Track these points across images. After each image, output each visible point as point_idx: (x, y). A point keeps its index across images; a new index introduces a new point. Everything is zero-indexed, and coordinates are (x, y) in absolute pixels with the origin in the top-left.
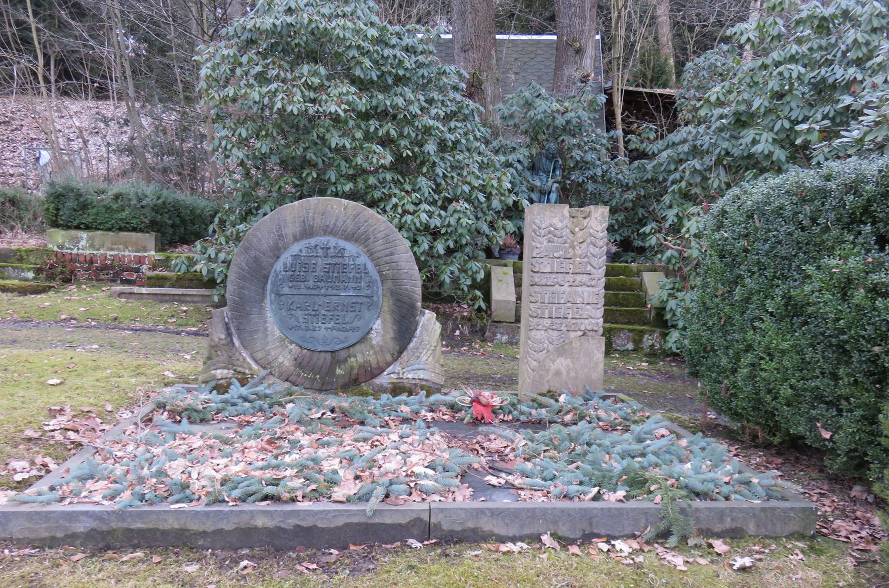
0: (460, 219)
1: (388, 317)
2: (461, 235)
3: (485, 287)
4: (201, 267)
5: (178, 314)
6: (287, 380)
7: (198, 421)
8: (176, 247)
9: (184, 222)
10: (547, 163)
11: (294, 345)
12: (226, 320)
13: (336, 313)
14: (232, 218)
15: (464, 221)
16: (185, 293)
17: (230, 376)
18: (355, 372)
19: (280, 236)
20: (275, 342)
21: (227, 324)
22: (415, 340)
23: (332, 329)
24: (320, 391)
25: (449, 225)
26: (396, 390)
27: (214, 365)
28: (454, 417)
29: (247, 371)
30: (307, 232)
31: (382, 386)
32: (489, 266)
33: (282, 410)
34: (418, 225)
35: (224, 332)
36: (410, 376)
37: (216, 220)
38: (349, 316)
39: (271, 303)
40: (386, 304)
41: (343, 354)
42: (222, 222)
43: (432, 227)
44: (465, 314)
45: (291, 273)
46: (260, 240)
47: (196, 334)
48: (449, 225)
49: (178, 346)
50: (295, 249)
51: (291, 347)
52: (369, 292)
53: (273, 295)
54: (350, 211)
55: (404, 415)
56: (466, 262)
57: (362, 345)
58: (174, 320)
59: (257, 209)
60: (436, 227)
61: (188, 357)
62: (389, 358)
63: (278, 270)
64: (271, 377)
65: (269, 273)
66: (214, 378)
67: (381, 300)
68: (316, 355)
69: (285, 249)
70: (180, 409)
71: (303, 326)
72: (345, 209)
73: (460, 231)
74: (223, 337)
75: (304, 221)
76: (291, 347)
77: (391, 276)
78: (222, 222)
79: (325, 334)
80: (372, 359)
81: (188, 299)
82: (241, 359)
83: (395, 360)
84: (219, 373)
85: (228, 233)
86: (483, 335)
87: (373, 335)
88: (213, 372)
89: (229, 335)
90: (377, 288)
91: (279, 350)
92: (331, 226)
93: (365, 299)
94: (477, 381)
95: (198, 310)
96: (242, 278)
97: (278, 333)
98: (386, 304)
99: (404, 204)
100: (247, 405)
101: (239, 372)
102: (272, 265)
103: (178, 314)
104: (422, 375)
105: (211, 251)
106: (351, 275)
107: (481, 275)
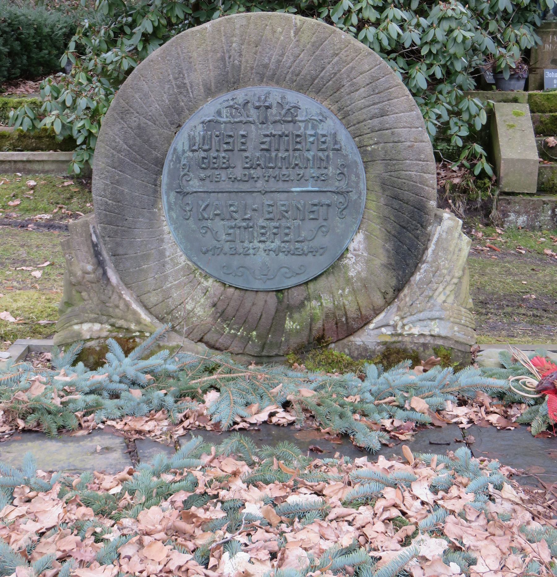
0: (451, 31)
1: (376, 227)
2: (455, 57)
3: (487, 137)
4: (52, 121)
5: (23, 192)
6: (201, 340)
7: (54, 432)
8: (17, 86)
9: (26, 47)
11: (211, 280)
12: (94, 239)
13: (284, 223)
14: (95, 41)
15: (459, 34)
16: (31, 158)
17: (105, 334)
18: (318, 325)
19: (182, 86)
20: (179, 278)
21: (95, 245)
22: (424, 266)
23: (277, 251)
24: (261, 359)
25: (434, 41)
26: (391, 356)
27: (77, 316)
28: (507, 417)
29: (133, 327)
30: (229, 79)
31: (366, 349)
32: (491, 102)
33: (196, 406)
34: (385, 43)
35: (93, 260)
36: (416, 331)
37: (72, 45)
38: (308, 229)
39: (170, 209)
40: (372, 205)
41: (296, 295)
42: (80, 50)
43: (407, 45)
44: (456, 181)
45: (203, 154)
46: (146, 95)
47: (49, 226)
48: (434, 41)
49: (23, 252)
50: (209, 109)
51: (206, 284)
52: (343, 185)
53: (173, 194)
54: (305, 38)
55: (417, 416)
56: (459, 99)
57: (331, 278)
58: (17, 202)
59: (132, 26)
60: (413, 44)
61: (38, 274)
62: (379, 300)
63: (180, 149)
64: (174, 334)
65: (165, 155)
66: (78, 338)
67: (364, 198)
68: (250, 297)
69: (191, 110)
70: (22, 407)
71: (227, 246)
72: (296, 33)
73: (452, 51)
74: (89, 268)
75: (223, 59)
76: (206, 284)
77: (382, 154)
78: (80, 50)
79: (266, 262)
80: (349, 302)
81: (36, 167)
82: (122, 306)
83: (389, 303)
84: (87, 329)
85: (91, 65)
86: (487, 215)
87: (350, 260)
88: (76, 327)
89: (100, 264)
90: (358, 176)
91: (187, 289)
92: (272, 66)
93: (335, 197)
94: (501, 307)
95: (51, 185)
96: (119, 165)
97: (182, 260)
98: (373, 205)
99: (360, 11)
100: (137, 393)
101: (120, 328)
102: (169, 140)
103: (23, 192)
104: (436, 328)
105: (67, 96)
106: (310, 155)
107: (482, 120)
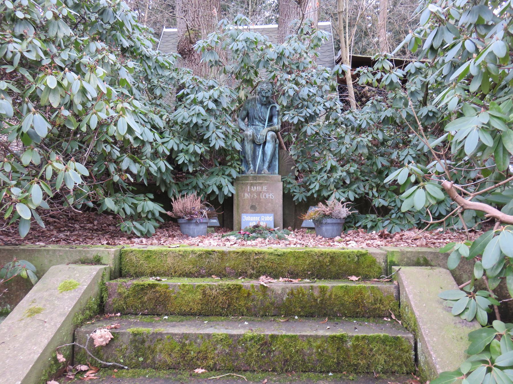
10: (263, 110)
